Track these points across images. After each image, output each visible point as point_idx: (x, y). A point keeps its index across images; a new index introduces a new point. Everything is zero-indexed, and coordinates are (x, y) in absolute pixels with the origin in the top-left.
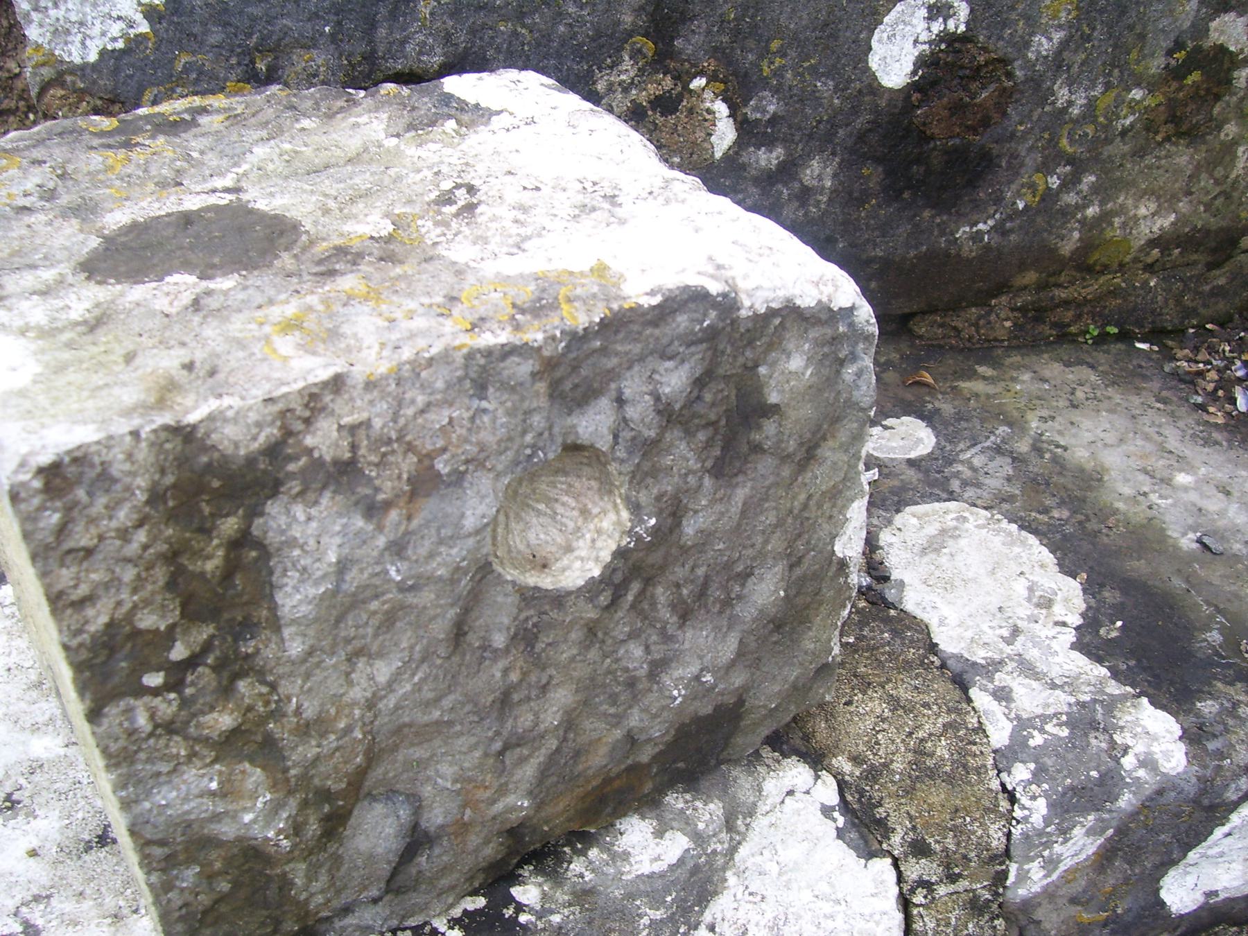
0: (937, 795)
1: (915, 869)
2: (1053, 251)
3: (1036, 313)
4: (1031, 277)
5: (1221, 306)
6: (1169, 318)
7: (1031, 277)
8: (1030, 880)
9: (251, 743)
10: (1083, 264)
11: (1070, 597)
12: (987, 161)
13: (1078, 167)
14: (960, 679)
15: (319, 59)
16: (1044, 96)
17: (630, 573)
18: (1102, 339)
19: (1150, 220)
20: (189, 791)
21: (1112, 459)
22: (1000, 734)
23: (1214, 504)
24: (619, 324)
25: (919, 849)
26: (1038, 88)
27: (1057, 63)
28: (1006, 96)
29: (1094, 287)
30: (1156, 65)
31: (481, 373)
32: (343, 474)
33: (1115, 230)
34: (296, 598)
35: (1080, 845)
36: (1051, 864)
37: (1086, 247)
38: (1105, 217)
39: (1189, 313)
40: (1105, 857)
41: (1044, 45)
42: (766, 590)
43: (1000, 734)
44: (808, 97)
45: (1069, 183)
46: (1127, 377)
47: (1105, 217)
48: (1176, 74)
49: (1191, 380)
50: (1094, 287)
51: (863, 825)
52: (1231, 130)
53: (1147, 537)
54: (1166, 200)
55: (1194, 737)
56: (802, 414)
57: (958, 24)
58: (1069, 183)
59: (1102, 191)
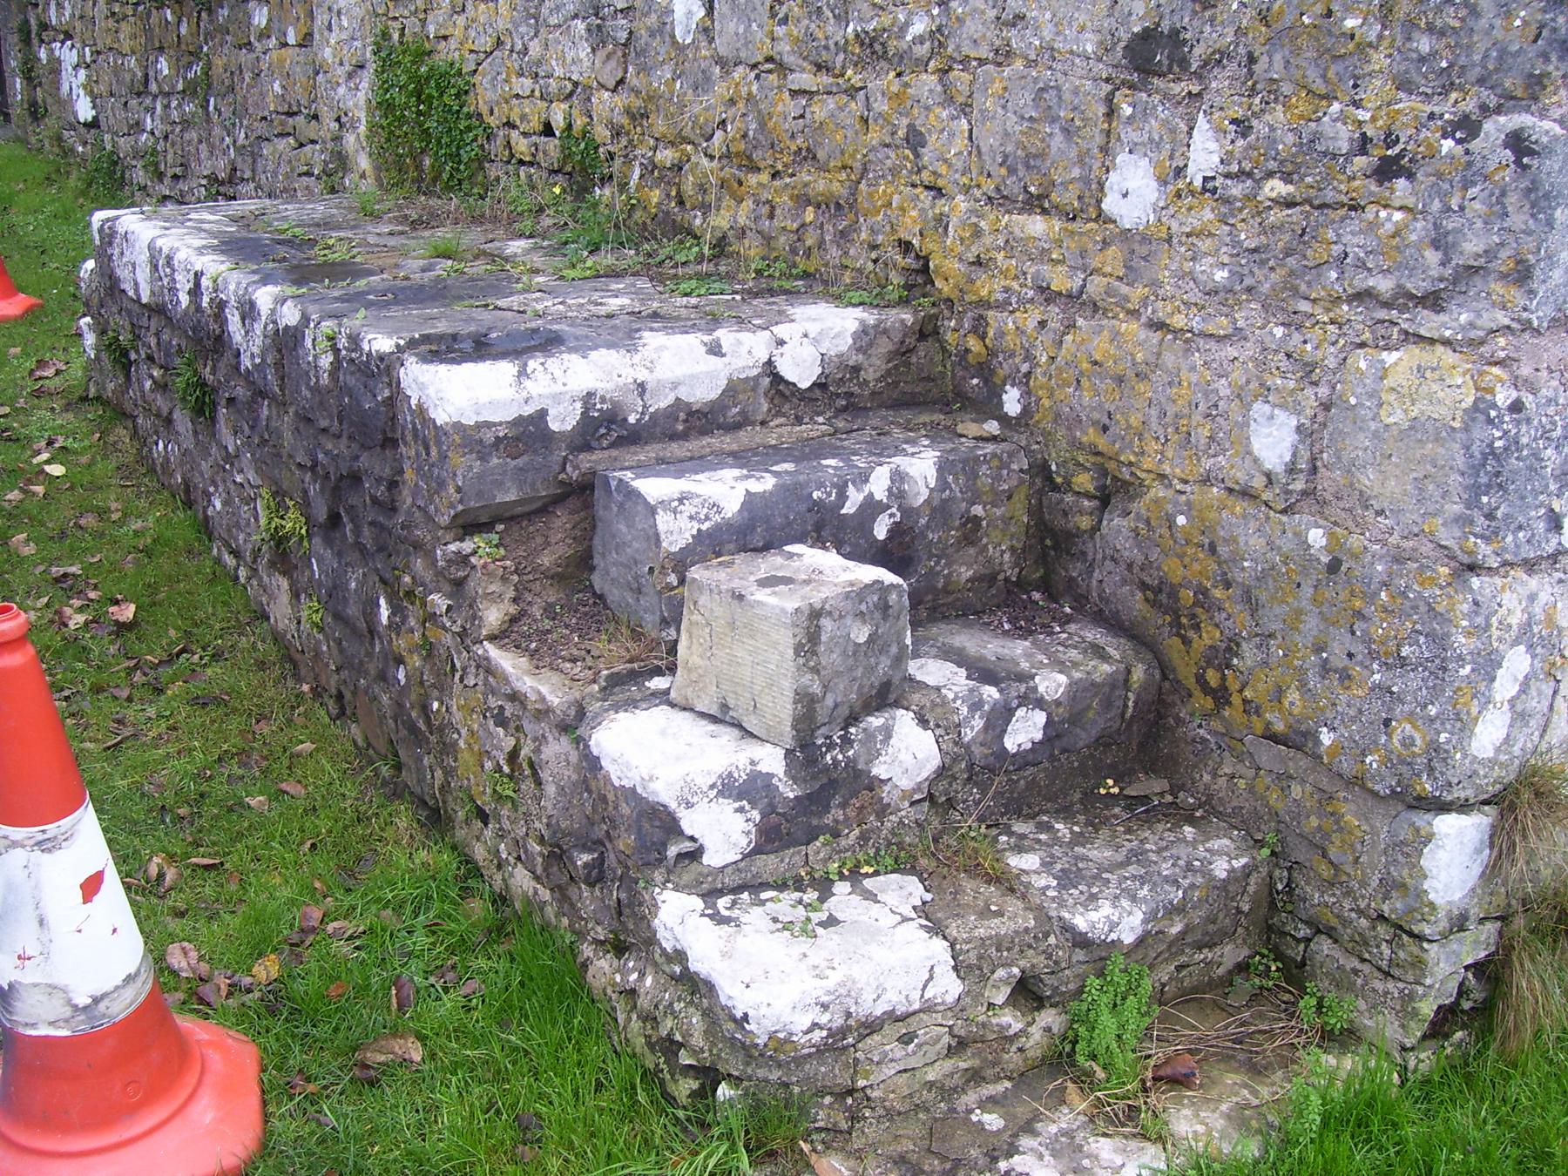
0: (939, 710)
1: (938, 732)
2: (935, 588)
3: (933, 609)
4: (930, 597)
5: (996, 601)
6: (979, 607)
7: (930, 597)
8: (968, 735)
9: (815, 670)
10: (946, 591)
11: (963, 672)
12: (911, 559)
13: (939, 558)
14: (938, 689)
15: (732, 546)
16: (926, 537)
17: (872, 639)
18: (957, 616)
19: (966, 573)
20: (807, 679)
21: (967, 644)
22: (951, 696)
23: (1000, 650)
24: (866, 586)
25: (938, 726)
26: (923, 535)
27: (928, 526)
28: (913, 538)
29: (951, 599)
30: (957, 523)
31: (847, 596)
32: (830, 613)
33: (955, 577)
34: (824, 638)
35: (978, 723)
36: (972, 728)
37: (946, 584)
38: (950, 574)
39: (985, 604)
40: (986, 728)
41: (923, 521)
42: (894, 649)
43: (951, 696)
44: (858, 545)
45: (937, 563)
46: (969, 625)
47: (950, 574)
48: (964, 525)
49: (989, 624)
50: (951, 599)
51: (923, 722)
52: (985, 540)
53: (982, 659)
54: (969, 566)
55: (1001, 691)
56: (896, 608)
57: (898, 519)
58: (937, 563)
59: (948, 565)
